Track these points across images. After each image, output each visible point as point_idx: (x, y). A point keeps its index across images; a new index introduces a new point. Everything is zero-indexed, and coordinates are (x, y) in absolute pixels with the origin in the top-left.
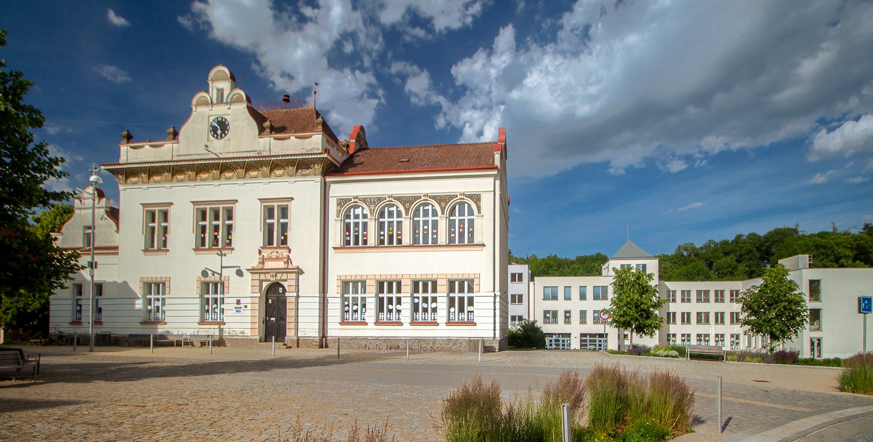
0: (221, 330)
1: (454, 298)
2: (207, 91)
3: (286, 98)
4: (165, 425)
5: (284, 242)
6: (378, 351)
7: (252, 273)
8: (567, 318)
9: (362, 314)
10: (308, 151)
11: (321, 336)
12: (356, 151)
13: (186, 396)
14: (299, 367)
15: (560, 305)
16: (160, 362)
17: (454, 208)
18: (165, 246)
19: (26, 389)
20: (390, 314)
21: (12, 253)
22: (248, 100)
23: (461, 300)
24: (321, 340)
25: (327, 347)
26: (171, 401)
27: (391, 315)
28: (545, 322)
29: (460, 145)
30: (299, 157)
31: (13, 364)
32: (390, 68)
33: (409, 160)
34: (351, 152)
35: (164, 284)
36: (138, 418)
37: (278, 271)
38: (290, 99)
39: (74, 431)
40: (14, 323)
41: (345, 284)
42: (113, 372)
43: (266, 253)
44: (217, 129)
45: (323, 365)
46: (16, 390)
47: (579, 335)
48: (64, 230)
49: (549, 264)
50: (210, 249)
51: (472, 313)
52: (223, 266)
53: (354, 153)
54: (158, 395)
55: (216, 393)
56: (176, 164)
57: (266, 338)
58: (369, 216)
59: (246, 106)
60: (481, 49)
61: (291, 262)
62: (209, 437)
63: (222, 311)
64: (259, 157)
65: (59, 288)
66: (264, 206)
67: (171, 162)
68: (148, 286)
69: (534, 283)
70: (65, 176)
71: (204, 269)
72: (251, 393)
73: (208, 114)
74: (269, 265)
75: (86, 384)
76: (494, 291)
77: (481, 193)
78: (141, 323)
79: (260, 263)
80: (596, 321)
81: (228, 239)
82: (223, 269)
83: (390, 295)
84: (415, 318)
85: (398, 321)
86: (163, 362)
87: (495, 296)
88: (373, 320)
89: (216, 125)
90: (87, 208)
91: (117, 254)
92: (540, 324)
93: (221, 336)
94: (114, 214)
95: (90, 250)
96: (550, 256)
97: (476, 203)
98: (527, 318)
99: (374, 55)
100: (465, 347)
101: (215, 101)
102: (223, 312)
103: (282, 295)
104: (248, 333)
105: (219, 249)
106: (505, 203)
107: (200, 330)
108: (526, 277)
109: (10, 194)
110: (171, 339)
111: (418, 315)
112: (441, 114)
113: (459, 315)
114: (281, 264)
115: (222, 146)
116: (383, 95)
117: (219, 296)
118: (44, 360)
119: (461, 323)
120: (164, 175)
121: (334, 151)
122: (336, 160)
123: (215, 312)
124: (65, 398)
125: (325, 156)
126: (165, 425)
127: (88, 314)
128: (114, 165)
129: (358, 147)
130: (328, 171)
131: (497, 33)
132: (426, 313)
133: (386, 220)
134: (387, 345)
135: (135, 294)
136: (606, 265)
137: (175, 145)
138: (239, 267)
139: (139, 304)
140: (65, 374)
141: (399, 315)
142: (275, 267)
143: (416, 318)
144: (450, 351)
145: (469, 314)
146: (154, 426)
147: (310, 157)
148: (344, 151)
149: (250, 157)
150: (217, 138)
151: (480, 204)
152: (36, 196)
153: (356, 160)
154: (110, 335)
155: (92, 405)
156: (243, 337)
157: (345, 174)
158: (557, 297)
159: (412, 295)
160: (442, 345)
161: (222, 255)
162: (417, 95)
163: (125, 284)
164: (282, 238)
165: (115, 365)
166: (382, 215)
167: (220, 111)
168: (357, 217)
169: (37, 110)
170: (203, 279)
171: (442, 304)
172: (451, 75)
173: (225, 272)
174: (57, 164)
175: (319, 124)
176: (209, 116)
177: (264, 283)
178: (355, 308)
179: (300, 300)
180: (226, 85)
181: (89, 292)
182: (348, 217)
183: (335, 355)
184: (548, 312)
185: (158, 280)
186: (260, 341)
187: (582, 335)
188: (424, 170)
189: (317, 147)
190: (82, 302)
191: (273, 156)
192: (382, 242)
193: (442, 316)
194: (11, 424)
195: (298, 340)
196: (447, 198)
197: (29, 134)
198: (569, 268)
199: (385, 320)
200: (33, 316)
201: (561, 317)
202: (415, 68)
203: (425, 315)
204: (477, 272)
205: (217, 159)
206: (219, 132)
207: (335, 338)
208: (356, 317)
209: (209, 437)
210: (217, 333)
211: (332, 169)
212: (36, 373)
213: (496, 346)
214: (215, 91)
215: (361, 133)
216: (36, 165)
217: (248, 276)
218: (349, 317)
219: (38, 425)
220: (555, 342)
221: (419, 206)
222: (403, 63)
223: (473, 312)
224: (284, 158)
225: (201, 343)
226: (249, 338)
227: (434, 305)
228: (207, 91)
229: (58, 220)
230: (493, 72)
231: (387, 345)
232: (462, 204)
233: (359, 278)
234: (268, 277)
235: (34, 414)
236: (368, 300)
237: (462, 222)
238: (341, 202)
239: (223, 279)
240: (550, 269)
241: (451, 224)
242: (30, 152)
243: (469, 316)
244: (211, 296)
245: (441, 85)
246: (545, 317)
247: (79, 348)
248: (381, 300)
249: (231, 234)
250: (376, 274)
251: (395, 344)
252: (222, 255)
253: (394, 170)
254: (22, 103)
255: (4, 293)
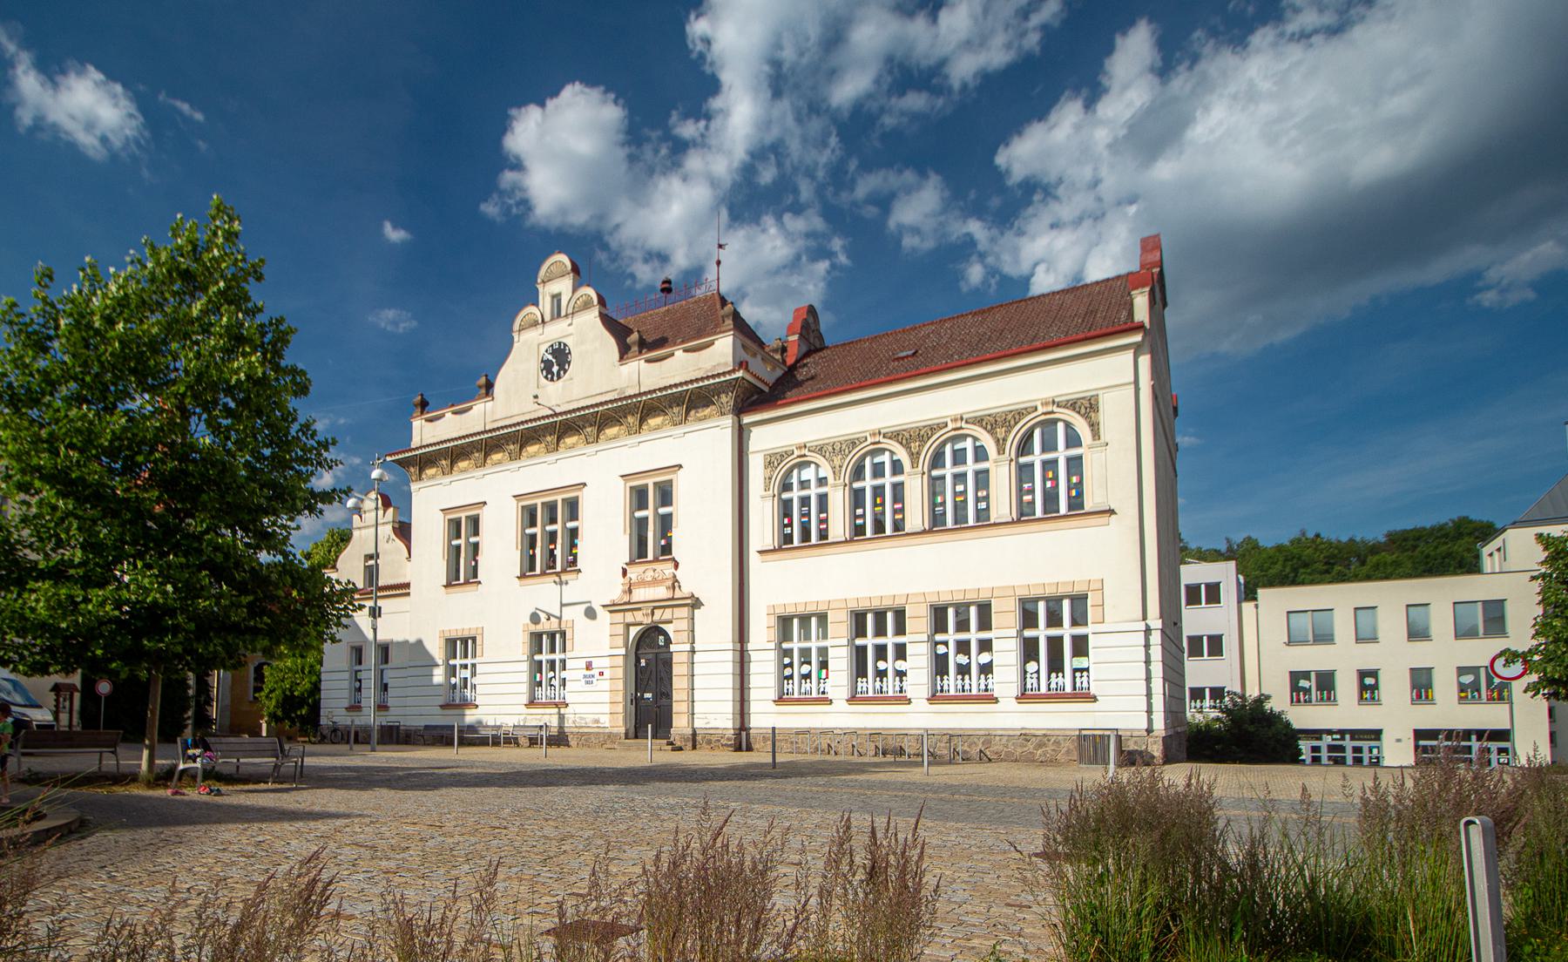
0: (561, 718)
1: (1036, 640)
2: (536, 304)
3: (666, 285)
4: (470, 856)
5: (667, 549)
6: (856, 759)
7: (611, 612)
8: (1368, 686)
9: (819, 683)
10: (707, 371)
11: (738, 726)
12: (800, 356)
13: (505, 816)
14: (697, 780)
15: (1344, 658)
16: (467, 767)
17: (1028, 437)
18: (475, 576)
19: (285, 796)
20: (881, 681)
21: (271, 588)
22: (602, 302)
23: (1055, 644)
24: (738, 735)
25: (749, 749)
26: (482, 822)
27: (885, 683)
28: (1295, 701)
29: (1039, 297)
30: (690, 387)
31: (272, 757)
32: (852, 190)
33: (916, 352)
34: (790, 360)
35: (474, 639)
36: (431, 843)
37: (657, 605)
38: (673, 286)
39: (340, 854)
40: (279, 713)
41: (784, 622)
42: (400, 778)
43: (634, 572)
44: (552, 364)
45: (744, 780)
46: (272, 795)
47: (1411, 735)
48: (339, 565)
49: (1299, 559)
50: (543, 574)
51: (1085, 674)
52: (564, 602)
53: (797, 361)
54: (463, 812)
55: (553, 813)
56: (490, 435)
57: (637, 732)
58: (831, 480)
59: (597, 313)
60: (1067, 93)
61: (680, 587)
62: (540, 879)
63: (564, 682)
64: (620, 399)
65: (329, 641)
66: (631, 488)
67: (482, 433)
68: (451, 644)
69: (1257, 606)
70: (337, 465)
71: (534, 610)
72: (611, 818)
73: (536, 343)
74: (640, 594)
75: (362, 793)
76: (1145, 618)
77: (1100, 392)
78: (441, 706)
79: (624, 592)
80: (1468, 692)
81: (571, 554)
82: (564, 608)
83: (880, 641)
84: (939, 688)
85: (899, 694)
86: (472, 768)
87: (1148, 631)
88: (845, 693)
89: (550, 357)
90: (368, 527)
91: (408, 594)
92: (1279, 703)
93: (561, 727)
94: (403, 531)
95: (371, 592)
96: (1299, 540)
97: (1086, 416)
98: (1238, 690)
99: (820, 174)
100: (1068, 752)
101: (547, 317)
102: (564, 686)
103: (664, 650)
104: (605, 721)
105: (558, 574)
106: (1167, 410)
107: (529, 717)
108: (1229, 593)
109: (269, 499)
110: (483, 732)
111: (945, 682)
112: (974, 258)
113: (1049, 678)
114: (661, 592)
115: (560, 390)
116: (843, 247)
117: (557, 656)
118: (308, 761)
119: (1057, 696)
120: (472, 457)
121: (756, 365)
122: (763, 381)
123: (551, 685)
124: (332, 809)
125: (740, 374)
126: (470, 856)
127: (370, 696)
128: (404, 452)
129: (804, 349)
130: (745, 405)
131: (1109, 49)
132: (967, 677)
133: (868, 483)
134: (876, 747)
135: (432, 659)
136: (1497, 542)
137: (489, 404)
138: (590, 602)
139: (439, 676)
140: (336, 779)
141: (901, 681)
142: (651, 598)
143: (942, 687)
144: (1030, 760)
145: (1078, 674)
146: (454, 856)
147: (712, 381)
148: (778, 360)
149: (606, 403)
150: (552, 380)
151: (1097, 417)
152: (300, 498)
153: (802, 374)
154: (398, 727)
155: (367, 820)
156: (597, 730)
157: (779, 402)
158: (1332, 635)
159: (931, 637)
160: (1007, 747)
161: (561, 583)
162: (916, 231)
163: (420, 643)
164: (663, 542)
165: (403, 769)
166: (858, 473)
167: (555, 332)
168: (804, 485)
169: (301, 370)
170: (533, 628)
171: (1006, 653)
172: (996, 168)
173: (568, 613)
174: (327, 450)
175: (727, 316)
176: (539, 345)
177: (631, 628)
178: (805, 669)
179: (697, 657)
180: (564, 286)
181: (371, 657)
182: (787, 487)
183: (767, 764)
184: (1306, 675)
185: (466, 634)
186: (627, 737)
187: (1419, 734)
188: (952, 365)
189: (723, 361)
190: (361, 675)
191: (645, 393)
192: (859, 530)
193: (1005, 679)
194: (261, 839)
195: (694, 734)
196: (1009, 417)
197: (291, 410)
198: (1363, 563)
199: (871, 694)
200: (301, 701)
201: (1346, 687)
202: (909, 176)
203: (963, 680)
204: (1096, 576)
205: (551, 416)
206: (555, 369)
207: (765, 731)
208: (808, 688)
209: (540, 879)
210: (554, 722)
211: (755, 397)
212: (298, 773)
213: (1157, 750)
214: (548, 299)
215: (811, 320)
216: (300, 453)
217: (603, 615)
218: (794, 687)
219: (294, 843)
220: (1329, 752)
221: (944, 444)
222: (882, 173)
223: (1087, 670)
224: (664, 393)
225: (530, 739)
226: (607, 730)
227: (985, 658)
228: (536, 304)
229: (333, 554)
230: (1102, 136)
231: (876, 747)
232: (1049, 425)
233: (811, 609)
234: (639, 616)
235: (291, 828)
236: (831, 653)
237: (1050, 465)
238: (772, 461)
239: (563, 626)
240: (1302, 570)
241: (1024, 472)
242: (293, 437)
243: (1078, 680)
244: (544, 657)
245: (972, 195)
246: (1295, 688)
247: (356, 747)
248: (861, 652)
249: (576, 546)
250: (848, 597)
251: (892, 743)
252: (561, 583)
253: (883, 378)
254: (283, 363)
255: (115, 330)
